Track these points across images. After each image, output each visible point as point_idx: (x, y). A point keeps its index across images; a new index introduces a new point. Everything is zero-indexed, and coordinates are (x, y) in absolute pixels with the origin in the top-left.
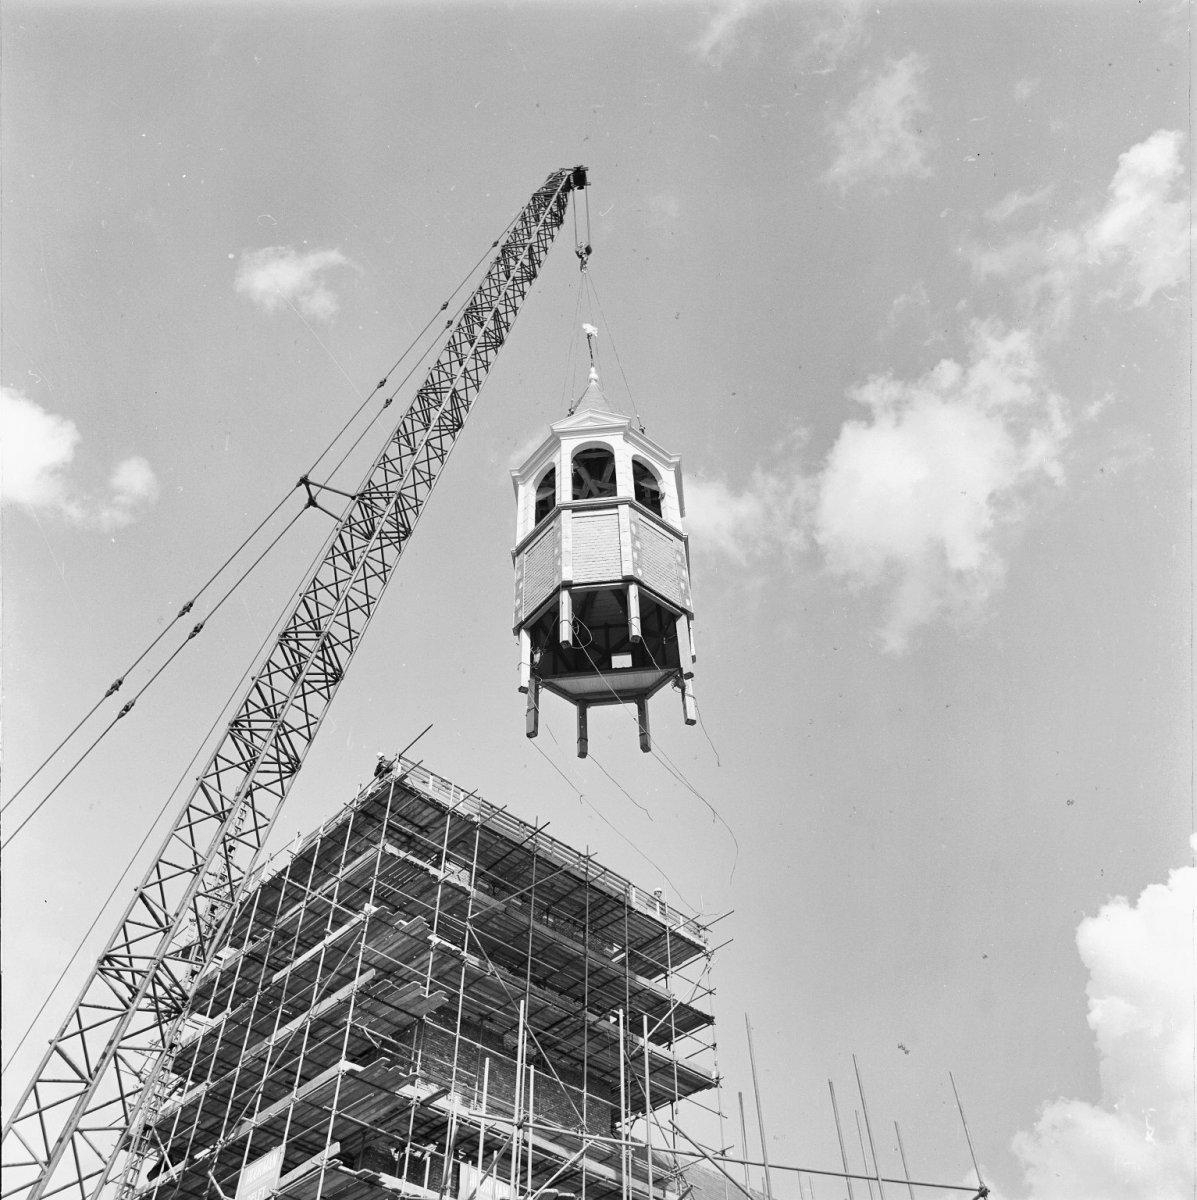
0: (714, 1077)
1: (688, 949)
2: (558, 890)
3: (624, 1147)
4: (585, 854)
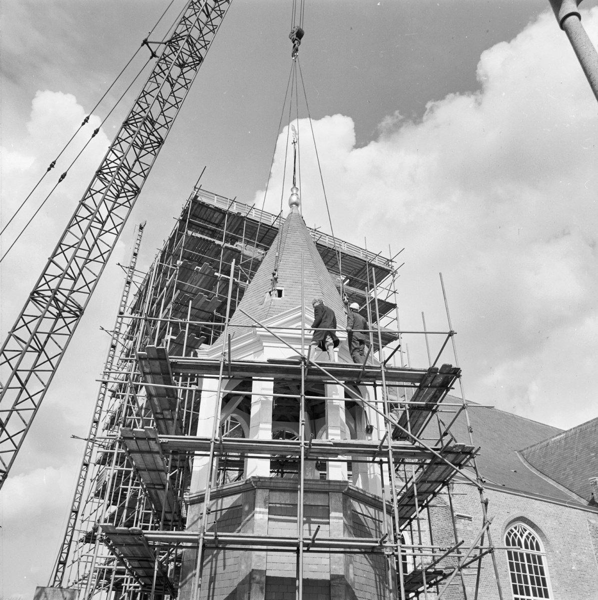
1: (383, 273)
4: (314, 228)
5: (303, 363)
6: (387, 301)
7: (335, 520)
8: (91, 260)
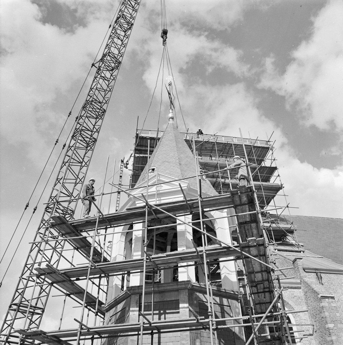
0: (280, 185)
2: (209, 148)
3: (260, 216)
5: (147, 207)
6: (272, 166)
7: (182, 309)
8: (77, 183)
